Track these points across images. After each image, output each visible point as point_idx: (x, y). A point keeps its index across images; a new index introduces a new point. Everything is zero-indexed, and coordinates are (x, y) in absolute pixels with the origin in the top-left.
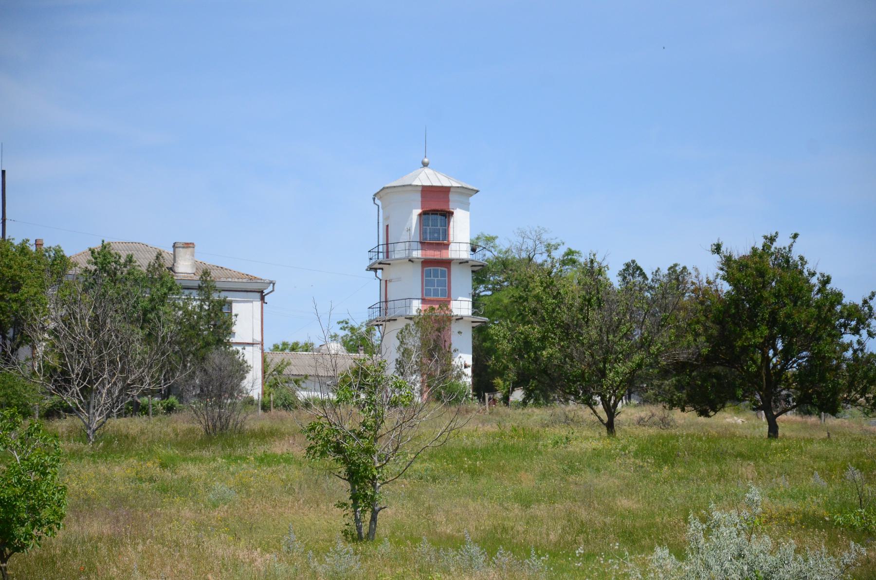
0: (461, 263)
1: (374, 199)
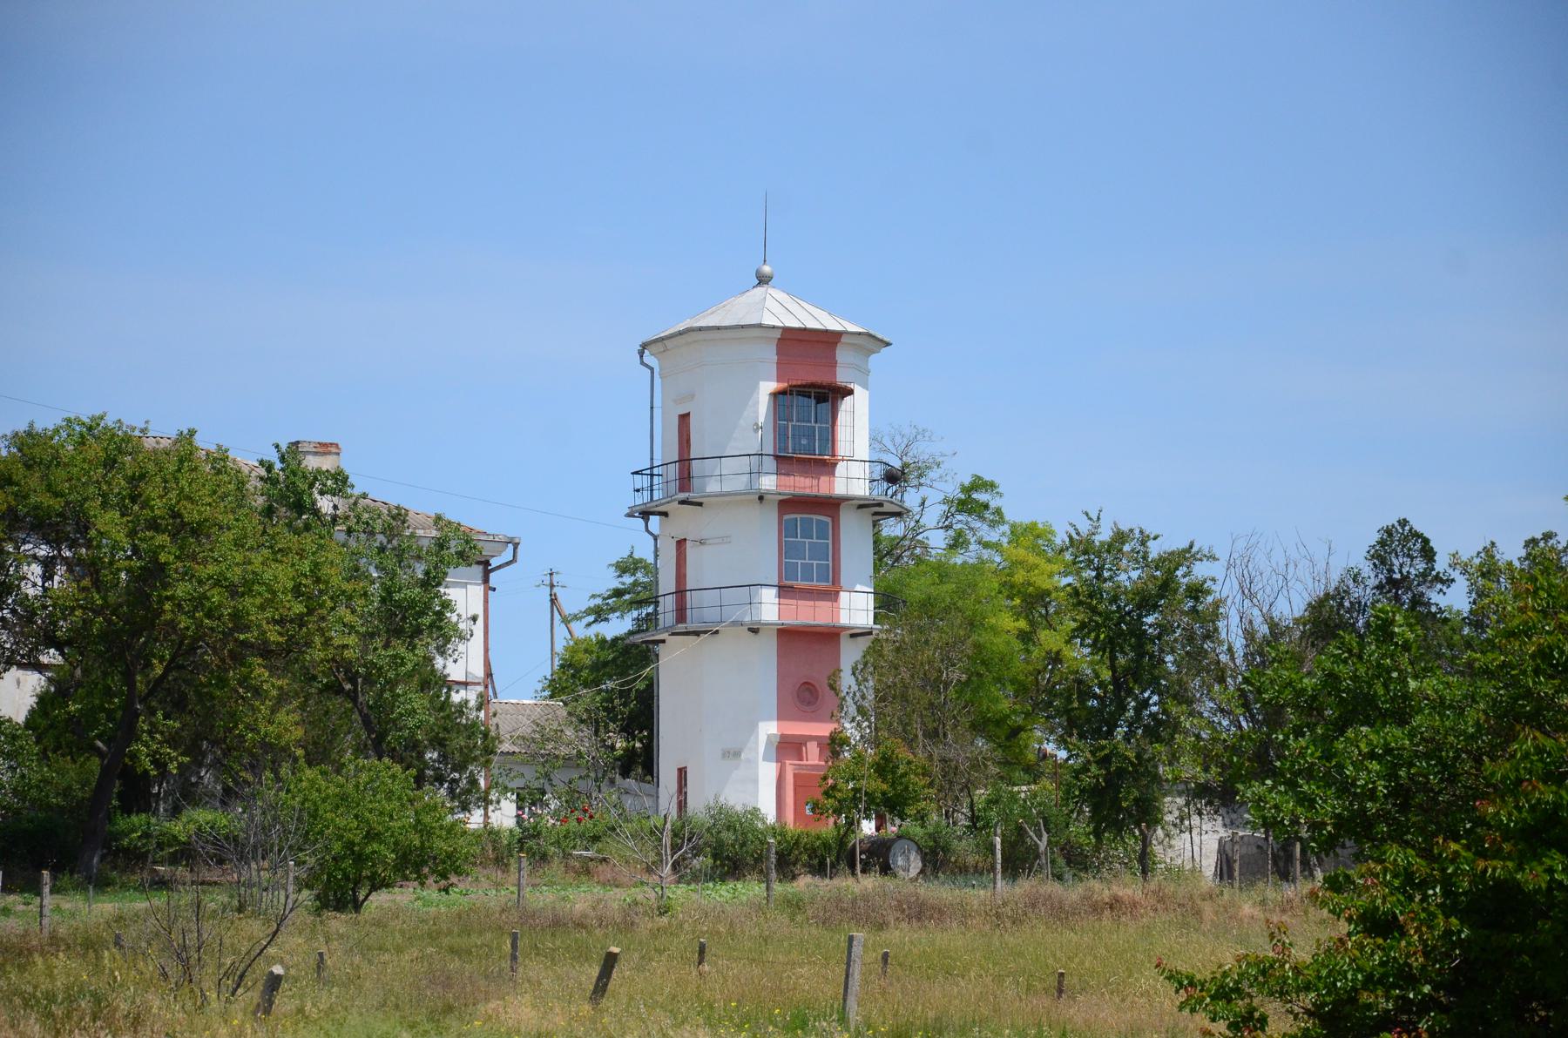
0: (860, 507)
1: (641, 354)
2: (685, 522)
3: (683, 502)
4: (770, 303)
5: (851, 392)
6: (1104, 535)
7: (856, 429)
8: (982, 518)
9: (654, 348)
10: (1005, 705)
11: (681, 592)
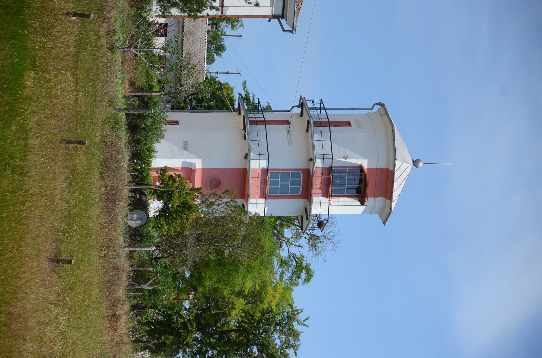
0: (306, 209)
2: (298, 125)
3: (309, 122)
4: (406, 165)
5: (362, 204)
6: (297, 327)
7: (344, 207)
8: (293, 274)
9: (382, 110)
10: (208, 283)
11: (265, 122)
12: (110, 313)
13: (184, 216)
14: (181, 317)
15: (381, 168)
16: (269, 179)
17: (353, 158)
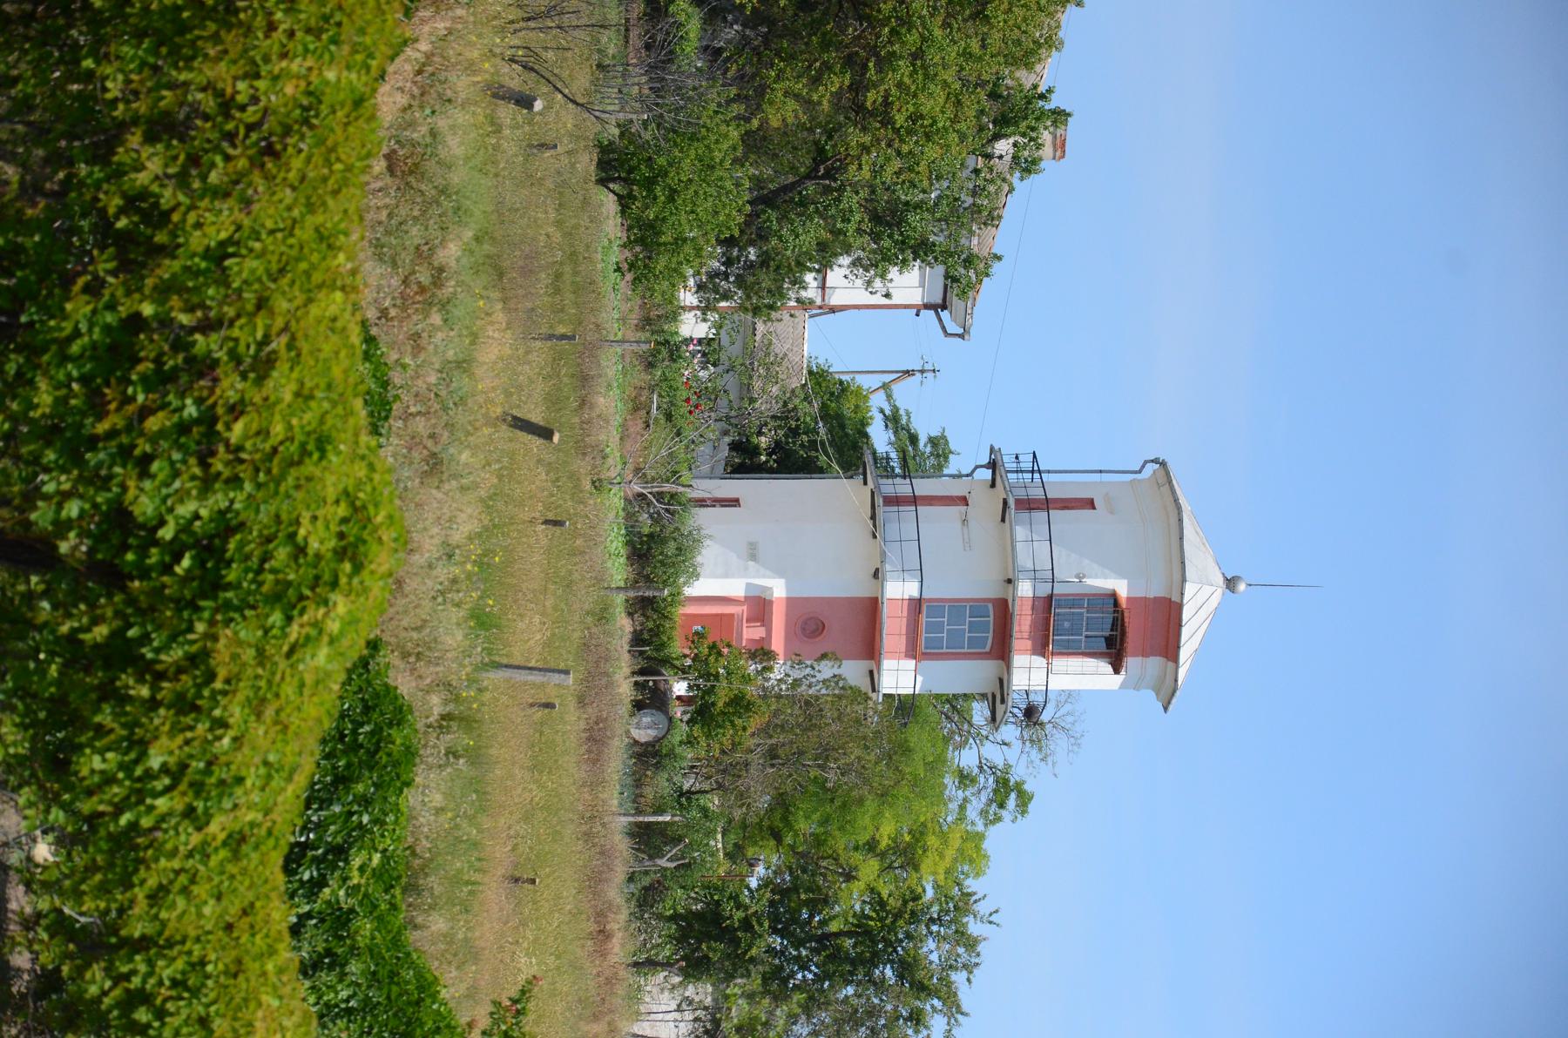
0: (1001, 681)
2: (985, 505)
3: (1005, 502)
4: (1207, 590)
5: (1117, 671)
6: (974, 928)
7: (1080, 677)
9: (1162, 472)
11: (914, 500)
12: (592, 927)
13: (738, 722)
14: (739, 906)
15: (1156, 599)
16: (924, 619)
17: (1096, 577)
